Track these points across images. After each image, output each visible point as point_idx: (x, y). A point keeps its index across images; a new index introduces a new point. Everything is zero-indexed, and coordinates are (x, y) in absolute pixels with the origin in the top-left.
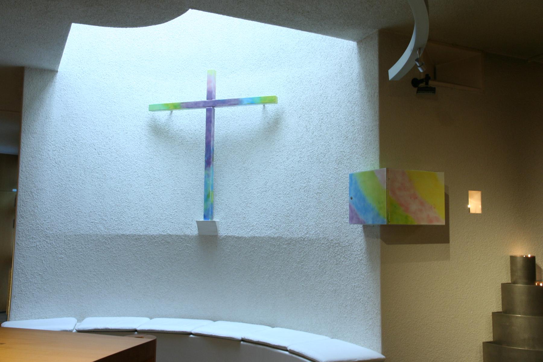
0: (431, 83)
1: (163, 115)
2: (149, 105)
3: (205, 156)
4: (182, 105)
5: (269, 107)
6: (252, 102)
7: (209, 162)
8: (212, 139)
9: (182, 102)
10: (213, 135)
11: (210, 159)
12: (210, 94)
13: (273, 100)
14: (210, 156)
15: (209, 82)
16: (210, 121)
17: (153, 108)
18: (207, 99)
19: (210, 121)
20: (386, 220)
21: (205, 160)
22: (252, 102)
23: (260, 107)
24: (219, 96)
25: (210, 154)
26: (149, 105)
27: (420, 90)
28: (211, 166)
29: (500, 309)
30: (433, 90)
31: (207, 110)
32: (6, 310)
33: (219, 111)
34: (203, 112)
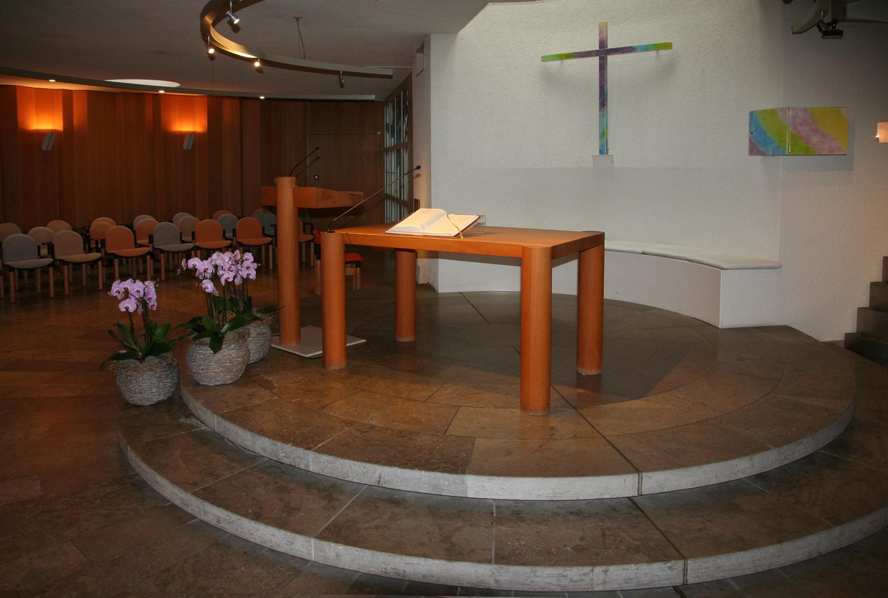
0: (839, 26)
1: (555, 64)
2: (542, 57)
3: (600, 99)
4: (574, 54)
5: (663, 53)
6: (646, 48)
7: (603, 103)
8: (605, 83)
9: (574, 52)
10: (607, 80)
11: (604, 101)
12: (603, 43)
13: (667, 46)
14: (604, 98)
15: (601, 33)
16: (603, 67)
17: (545, 59)
18: (600, 48)
19: (603, 67)
20: (637, 492)
21: (600, 103)
22: (646, 48)
23: (652, 54)
24: (610, 46)
25: (604, 96)
26: (542, 57)
27: (825, 34)
28: (605, 107)
29: (867, 305)
30: (840, 33)
31: (600, 58)
32: (434, 208)
33: (610, 58)
34: (596, 60)
